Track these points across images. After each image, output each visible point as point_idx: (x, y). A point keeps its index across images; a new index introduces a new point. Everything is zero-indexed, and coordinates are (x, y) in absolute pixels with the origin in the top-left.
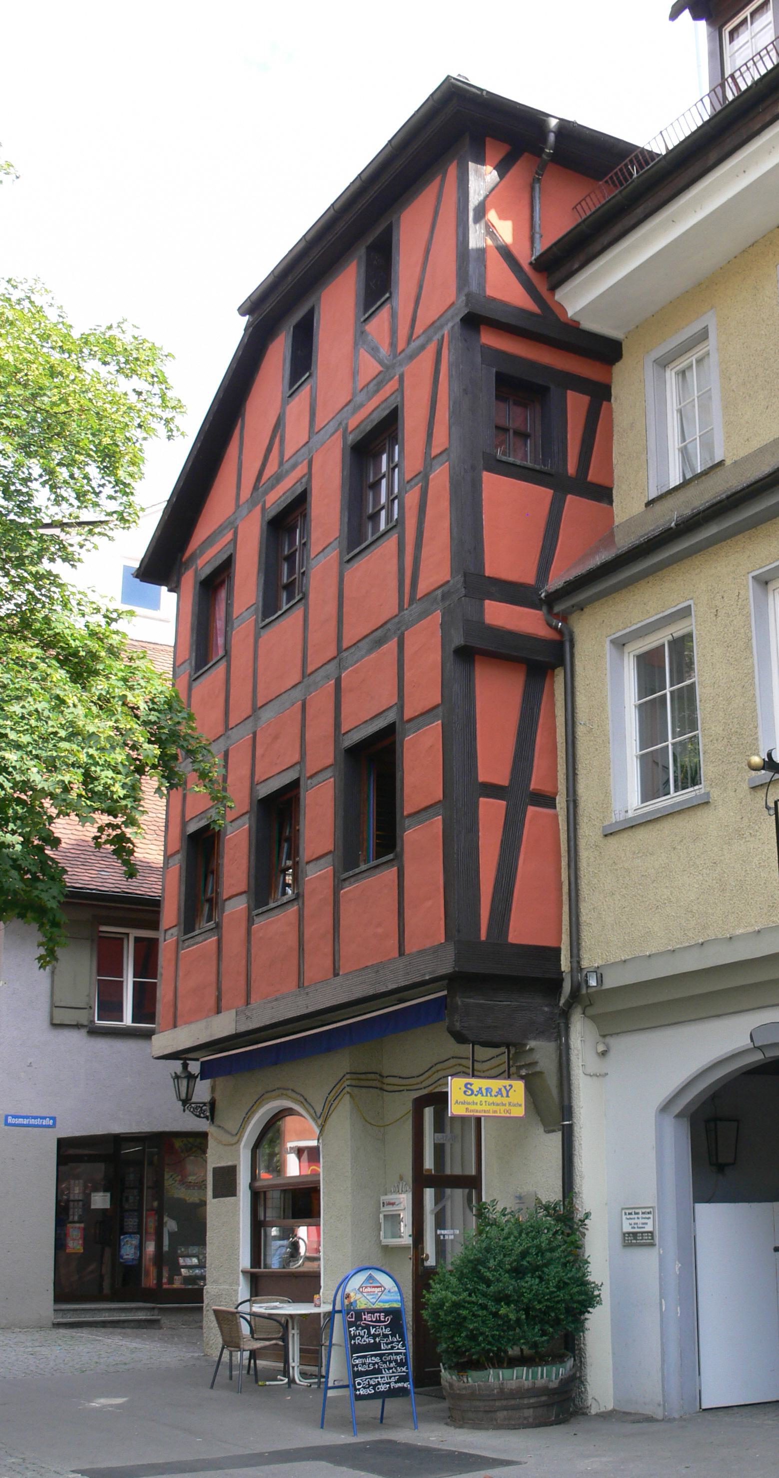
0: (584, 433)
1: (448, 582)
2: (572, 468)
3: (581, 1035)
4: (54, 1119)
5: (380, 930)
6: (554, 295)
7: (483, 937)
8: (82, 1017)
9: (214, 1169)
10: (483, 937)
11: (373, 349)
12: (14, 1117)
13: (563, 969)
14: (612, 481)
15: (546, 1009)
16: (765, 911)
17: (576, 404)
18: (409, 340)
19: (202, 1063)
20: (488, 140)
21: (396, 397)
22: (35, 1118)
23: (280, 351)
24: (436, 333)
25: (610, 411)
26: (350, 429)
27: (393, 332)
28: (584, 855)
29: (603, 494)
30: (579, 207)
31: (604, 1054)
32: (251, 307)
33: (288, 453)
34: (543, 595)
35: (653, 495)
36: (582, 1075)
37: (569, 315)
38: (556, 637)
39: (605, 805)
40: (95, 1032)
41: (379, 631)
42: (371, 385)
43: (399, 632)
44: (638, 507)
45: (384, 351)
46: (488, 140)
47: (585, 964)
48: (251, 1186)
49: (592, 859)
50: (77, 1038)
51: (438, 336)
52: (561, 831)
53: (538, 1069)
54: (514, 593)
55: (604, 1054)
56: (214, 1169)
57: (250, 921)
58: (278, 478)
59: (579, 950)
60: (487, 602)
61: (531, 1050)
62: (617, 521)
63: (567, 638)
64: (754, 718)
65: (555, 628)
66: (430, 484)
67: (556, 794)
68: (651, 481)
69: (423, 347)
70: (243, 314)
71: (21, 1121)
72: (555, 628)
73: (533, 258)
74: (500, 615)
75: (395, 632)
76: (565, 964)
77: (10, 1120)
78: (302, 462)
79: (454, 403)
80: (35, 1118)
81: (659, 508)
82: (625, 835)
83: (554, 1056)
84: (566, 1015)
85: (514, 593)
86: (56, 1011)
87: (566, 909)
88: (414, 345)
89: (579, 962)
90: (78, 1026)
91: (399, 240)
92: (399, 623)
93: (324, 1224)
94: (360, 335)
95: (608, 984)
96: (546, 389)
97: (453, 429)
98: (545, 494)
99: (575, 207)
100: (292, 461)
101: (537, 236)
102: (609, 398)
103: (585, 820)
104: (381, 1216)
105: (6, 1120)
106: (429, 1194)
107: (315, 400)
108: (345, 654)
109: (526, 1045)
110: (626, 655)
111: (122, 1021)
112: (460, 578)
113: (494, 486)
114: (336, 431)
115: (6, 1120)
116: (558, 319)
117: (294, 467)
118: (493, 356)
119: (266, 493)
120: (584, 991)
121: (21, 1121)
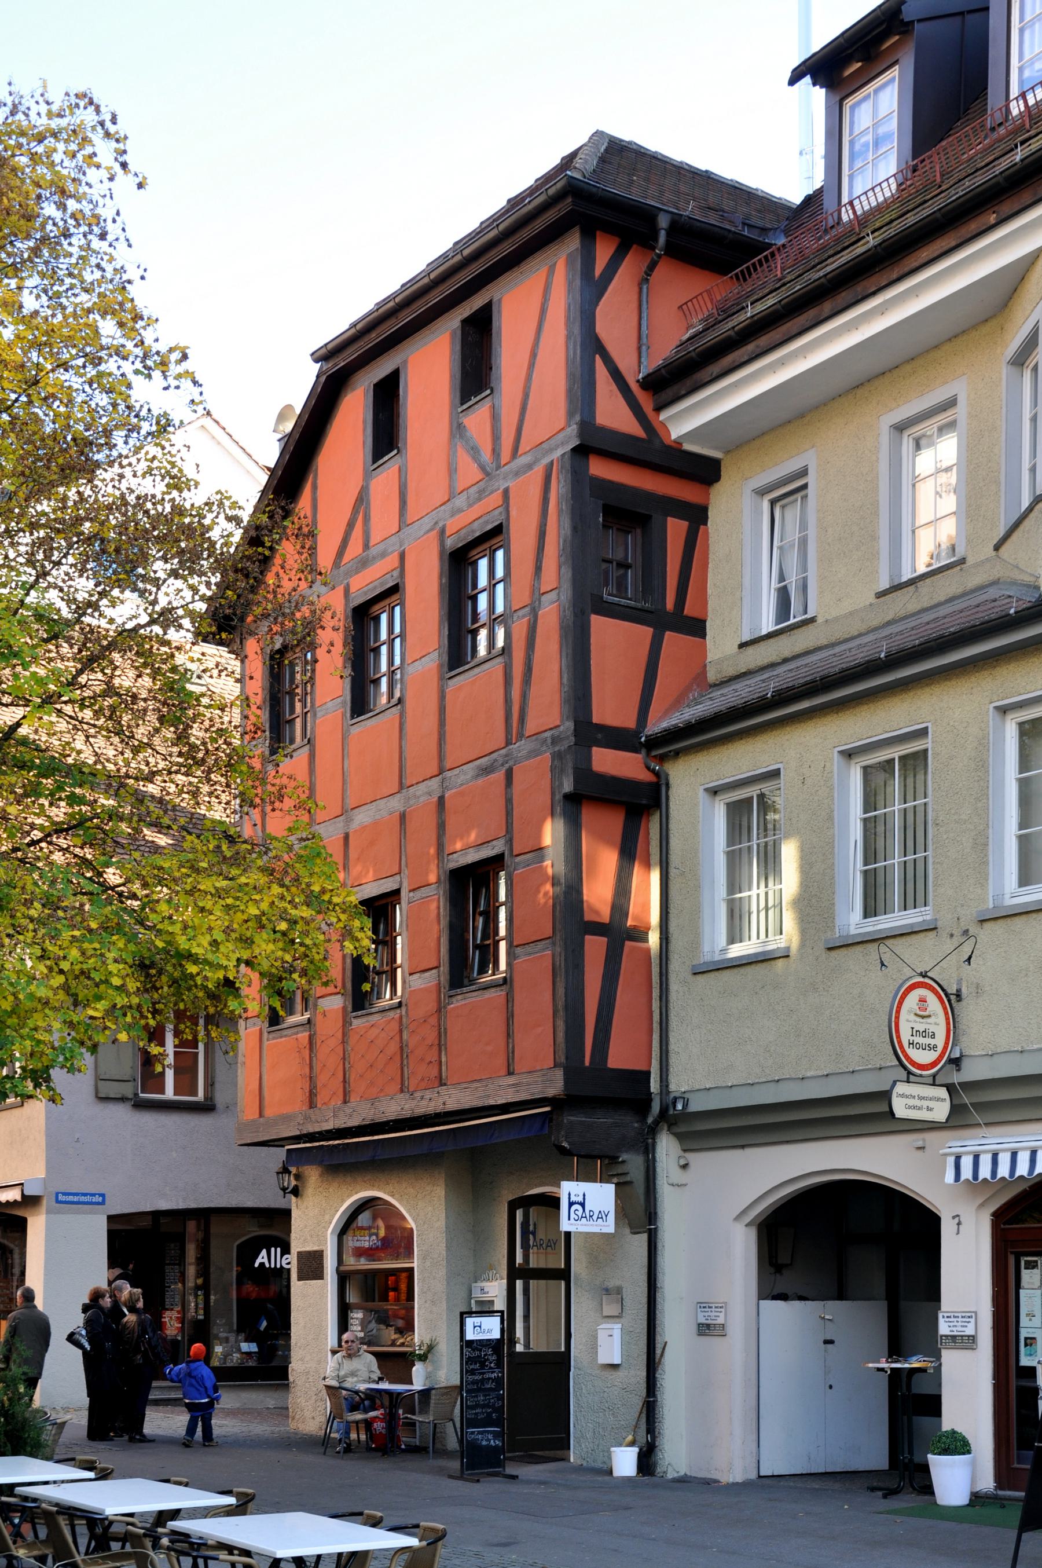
0: (682, 563)
1: (558, 726)
2: (670, 604)
3: (667, 1148)
4: (103, 1195)
5: (489, 1048)
6: (658, 415)
7: (587, 1063)
8: (127, 1090)
9: (299, 1253)
10: (587, 1063)
11: (472, 448)
12: (64, 1194)
13: (652, 1090)
14: (707, 616)
15: (636, 1125)
16: (834, 1057)
17: (676, 529)
18: (515, 453)
19: (288, 1150)
20: (598, 233)
21: (501, 513)
22: (85, 1195)
23: (355, 409)
24: (544, 456)
25: (707, 533)
26: (448, 533)
27: (496, 437)
28: (674, 987)
29: (697, 628)
30: (684, 307)
31: (685, 1167)
32: (324, 355)
33: (375, 539)
34: (643, 739)
35: (746, 638)
36: (666, 1186)
37: (673, 437)
38: (653, 779)
39: (695, 944)
40: (140, 1105)
41: (486, 759)
42: (472, 490)
43: (507, 765)
44: (732, 647)
45: (486, 456)
46: (598, 233)
47: (672, 1087)
48: (338, 1271)
49: (681, 993)
50: (122, 1113)
51: (545, 461)
52: (653, 965)
53: (628, 1178)
54: (619, 739)
55: (685, 1167)
56: (299, 1253)
57: (346, 1023)
58: (363, 563)
59: (667, 1076)
60: (594, 749)
61: (623, 1162)
62: (710, 657)
63: (663, 781)
64: (832, 884)
65: (653, 771)
66: (539, 621)
67: (649, 929)
68: (744, 621)
69: (530, 466)
70: (316, 361)
71: (71, 1198)
72: (653, 771)
73: (641, 376)
74: (608, 761)
75: (502, 765)
76: (654, 1086)
77: (61, 1197)
78: (392, 552)
79: (565, 541)
80: (85, 1195)
81: (750, 650)
82: (712, 975)
83: (642, 1169)
84: (653, 1131)
85: (619, 739)
86: (101, 1083)
87: (656, 1037)
88: (522, 460)
89: (667, 1086)
90: (123, 1099)
91: (500, 328)
92: (506, 756)
93: (419, 1308)
94: (458, 430)
95: (693, 1107)
96: (649, 517)
97: (563, 570)
98: (646, 632)
99: (680, 307)
100: (382, 546)
101: (644, 348)
102: (706, 524)
103: (676, 957)
104: (473, 1301)
105: (57, 1197)
106: (519, 1284)
107: (406, 487)
108: (449, 774)
109: (618, 1157)
110: (717, 806)
111: (164, 1093)
112: (570, 725)
113: (604, 630)
114: (431, 530)
115: (57, 1197)
116: (662, 442)
117: (383, 555)
118: (601, 486)
119: (348, 574)
120: (671, 1112)
121: (71, 1198)
